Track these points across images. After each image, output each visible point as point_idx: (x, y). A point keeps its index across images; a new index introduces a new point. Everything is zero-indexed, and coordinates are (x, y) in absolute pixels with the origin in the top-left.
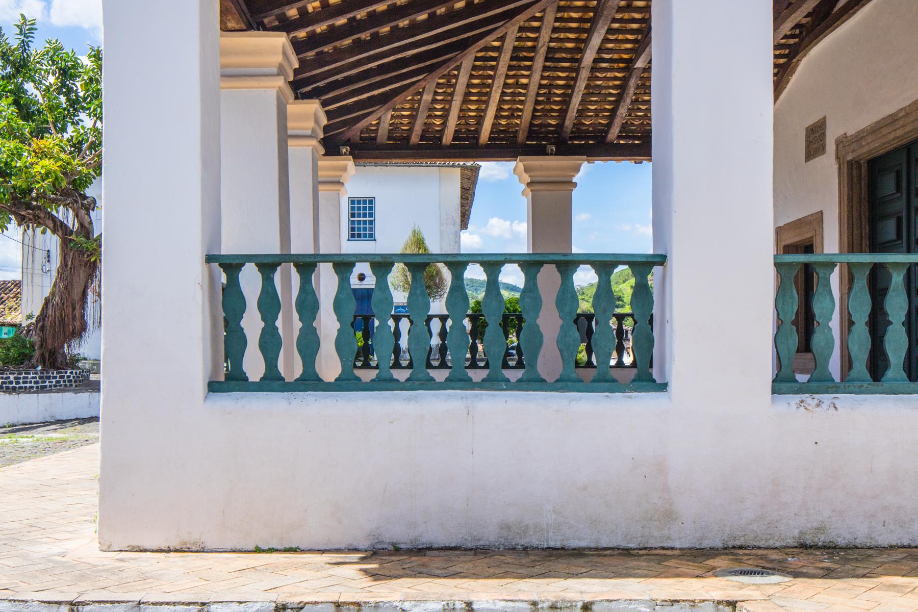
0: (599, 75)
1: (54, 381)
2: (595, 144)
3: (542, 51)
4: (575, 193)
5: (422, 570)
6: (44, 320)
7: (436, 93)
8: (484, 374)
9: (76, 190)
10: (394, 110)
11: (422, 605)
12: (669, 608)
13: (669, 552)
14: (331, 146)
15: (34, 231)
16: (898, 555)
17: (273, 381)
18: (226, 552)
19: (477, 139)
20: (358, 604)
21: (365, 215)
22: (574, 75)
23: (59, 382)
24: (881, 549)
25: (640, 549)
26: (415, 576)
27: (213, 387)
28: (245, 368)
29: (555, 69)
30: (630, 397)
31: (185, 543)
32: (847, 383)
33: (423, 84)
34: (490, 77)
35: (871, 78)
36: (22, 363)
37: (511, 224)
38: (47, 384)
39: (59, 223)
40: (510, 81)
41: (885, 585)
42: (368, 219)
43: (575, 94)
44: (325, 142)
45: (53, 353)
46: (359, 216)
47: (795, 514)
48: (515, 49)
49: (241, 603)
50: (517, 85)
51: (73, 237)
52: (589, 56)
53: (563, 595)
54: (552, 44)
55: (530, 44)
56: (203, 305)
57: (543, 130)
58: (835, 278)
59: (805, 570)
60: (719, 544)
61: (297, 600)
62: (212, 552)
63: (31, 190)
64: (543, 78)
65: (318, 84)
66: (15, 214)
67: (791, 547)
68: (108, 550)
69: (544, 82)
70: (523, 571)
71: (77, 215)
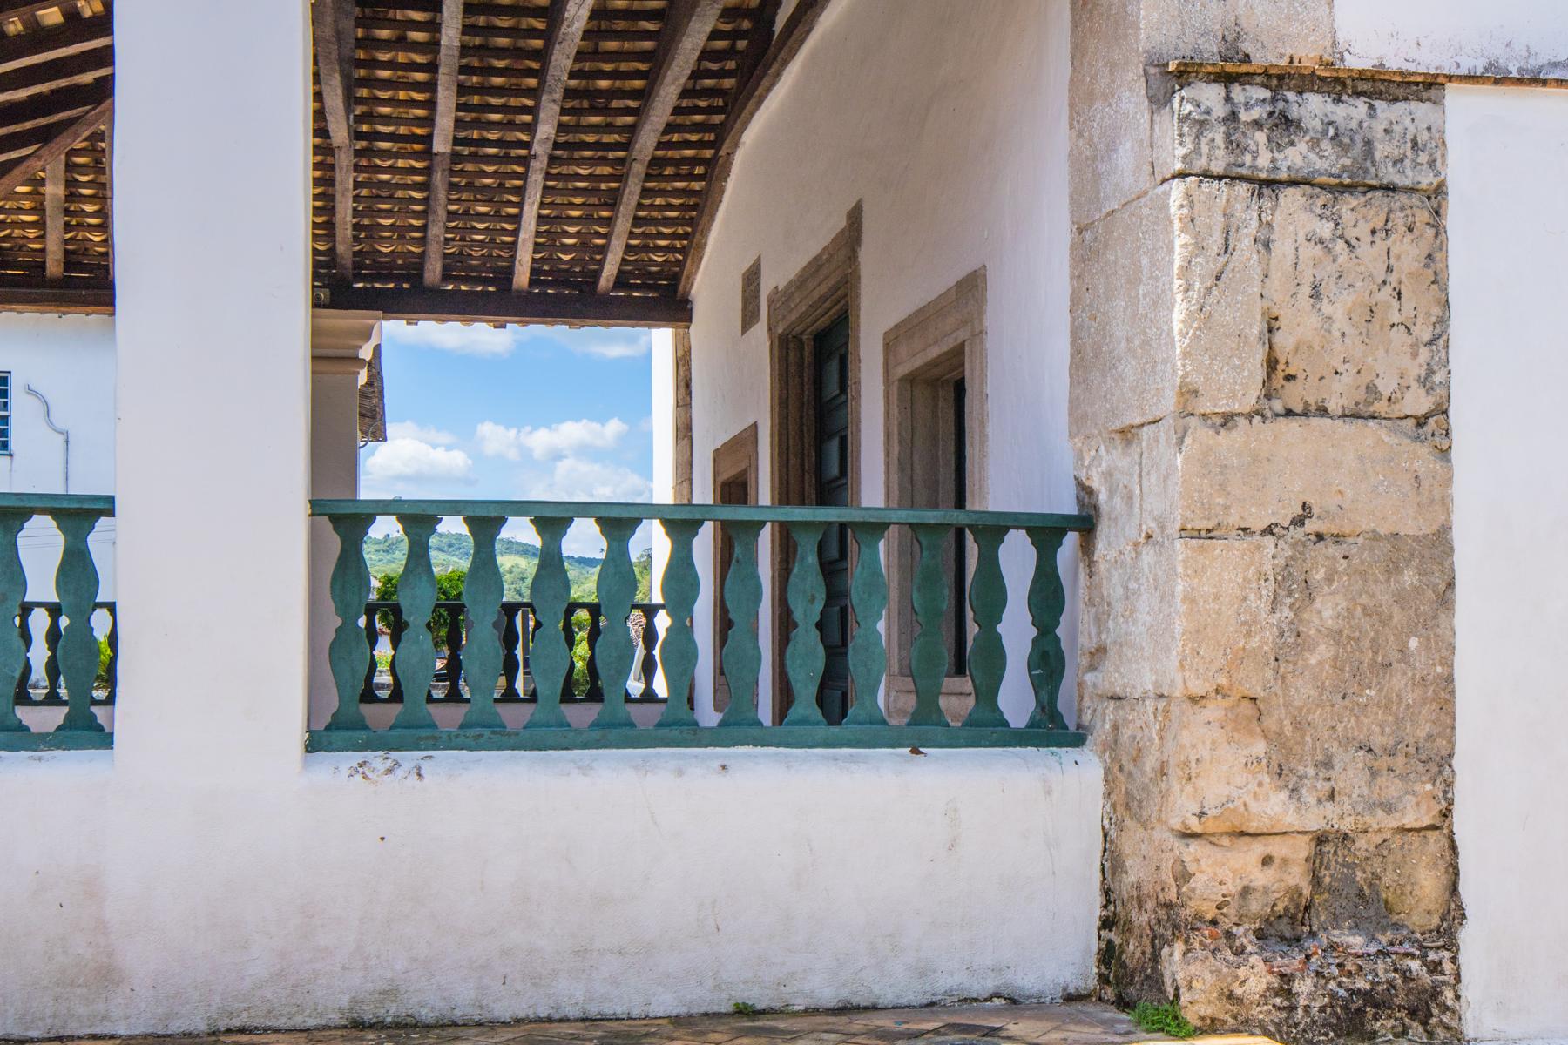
0: (378, 162)
8: (57, 715)
30: (40, 759)
47: (343, 968)
58: (765, 538)
67: (336, 1028)
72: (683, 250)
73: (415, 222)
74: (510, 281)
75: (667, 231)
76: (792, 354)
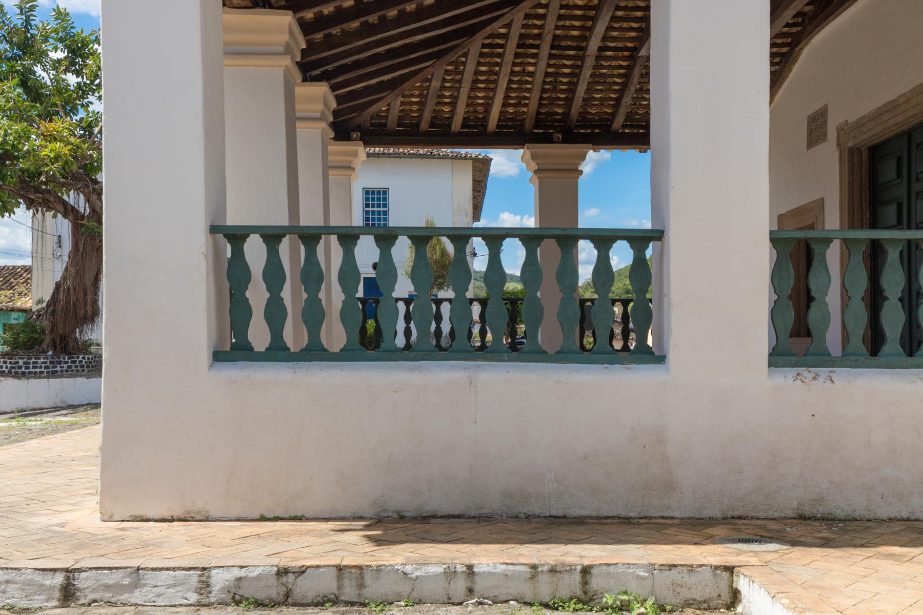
1: (65, 366)
2: (604, 134)
3: (548, 39)
4: (581, 180)
5: (425, 536)
6: (55, 305)
7: (444, 80)
9: (88, 175)
10: (403, 96)
11: (424, 568)
12: (667, 573)
13: (669, 522)
14: (342, 130)
15: (43, 215)
16: (897, 527)
17: (277, 352)
18: (230, 521)
19: (485, 127)
20: (360, 567)
21: (379, 206)
22: (579, 63)
23: (71, 367)
24: (880, 521)
25: (641, 518)
26: (417, 542)
27: (218, 357)
28: (251, 337)
29: (562, 57)
31: (189, 512)
32: (848, 360)
33: (431, 70)
34: (497, 64)
35: (871, 66)
36: (32, 348)
37: (521, 218)
38: (58, 369)
39: (69, 208)
40: (517, 69)
41: (883, 555)
42: (382, 209)
43: (580, 82)
44: (335, 126)
45: (64, 339)
46: (373, 206)
48: (522, 36)
49: (242, 567)
50: (524, 73)
51: (85, 222)
52: (594, 45)
53: (563, 558)
54: (558, 32)
55: (536, 31)
56: (207, 274)
57: (549, 118)
59: (803, 539)
60: (718, 514)
61: (299, 563)
62: (216, 520)
63: (40, 174)
64: (549, 66)
65: (327, 67)
66: (23, 197)
68: (110, 520)
69: (550, 70)
70: (525, 537)
71: (88, 200)
76: (855, 158)
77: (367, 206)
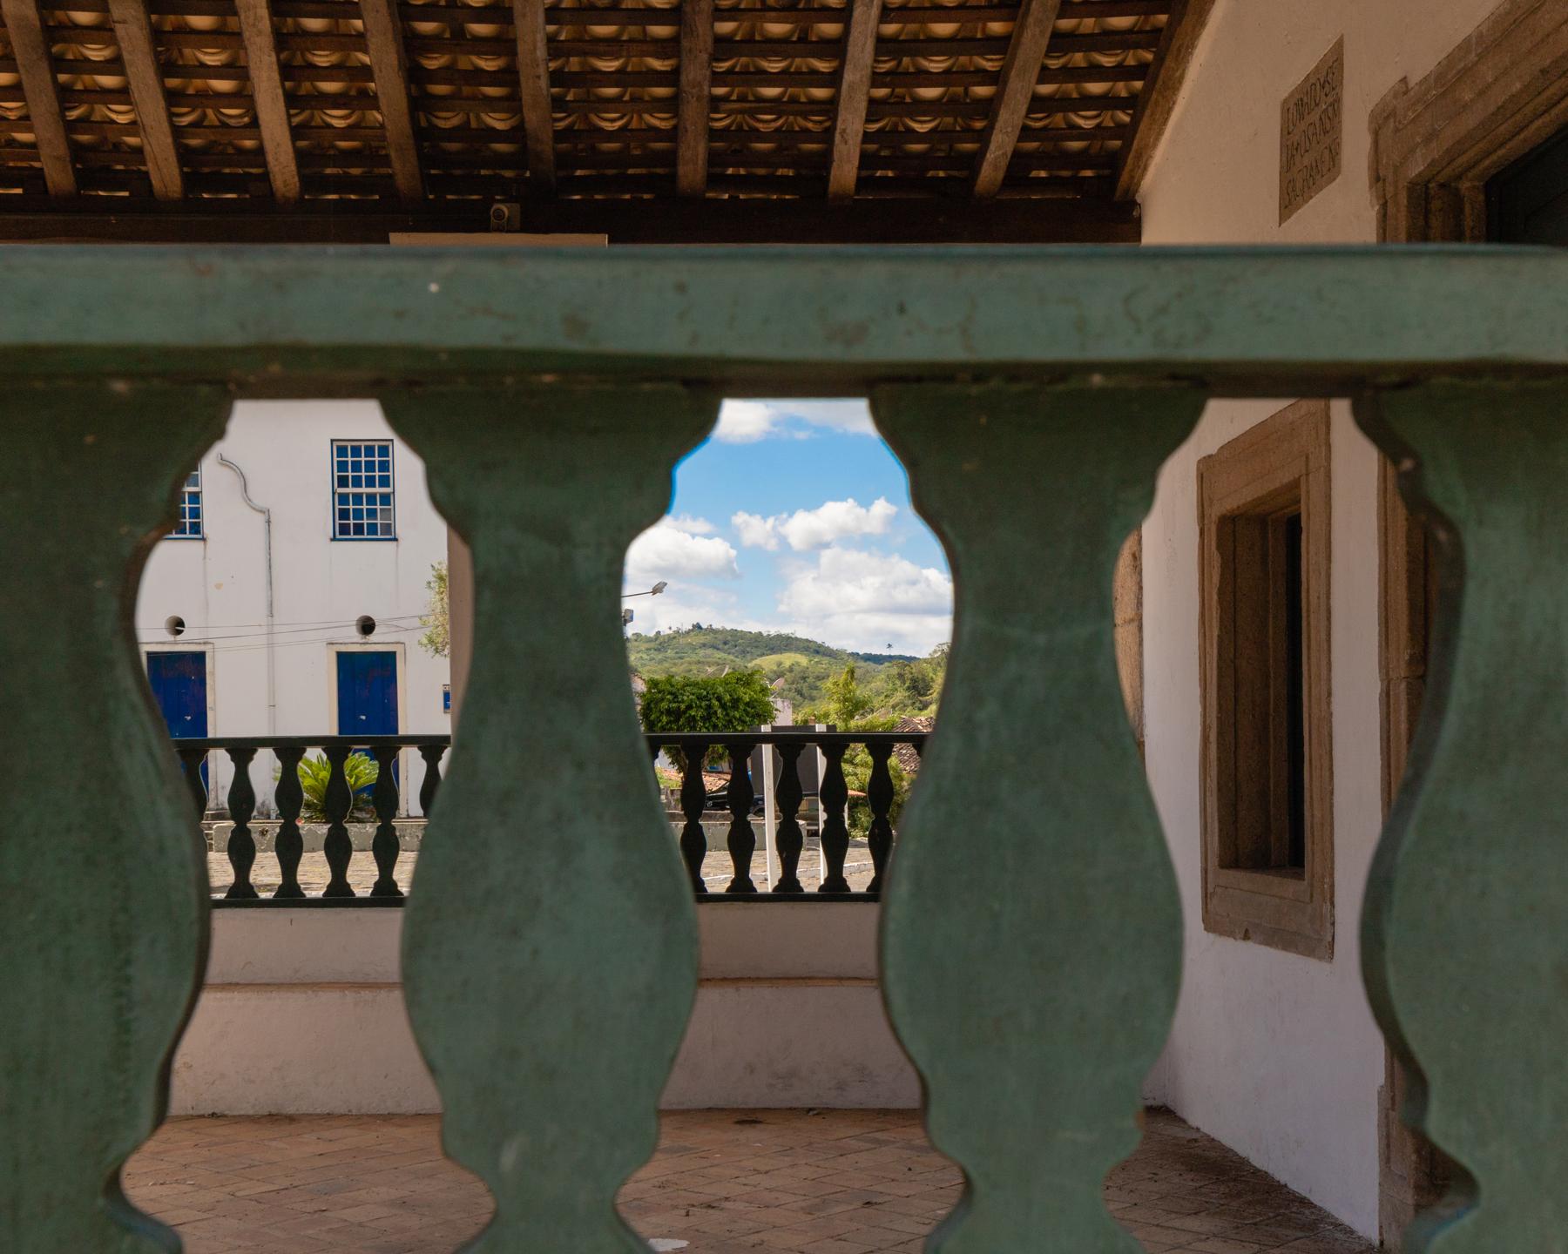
21: (370, 482)
42: (377, 490)
72: (1134, 103)
73: (657, 64)
74: (825, 181)
75: (1107, 61)
77: (343, 482)
